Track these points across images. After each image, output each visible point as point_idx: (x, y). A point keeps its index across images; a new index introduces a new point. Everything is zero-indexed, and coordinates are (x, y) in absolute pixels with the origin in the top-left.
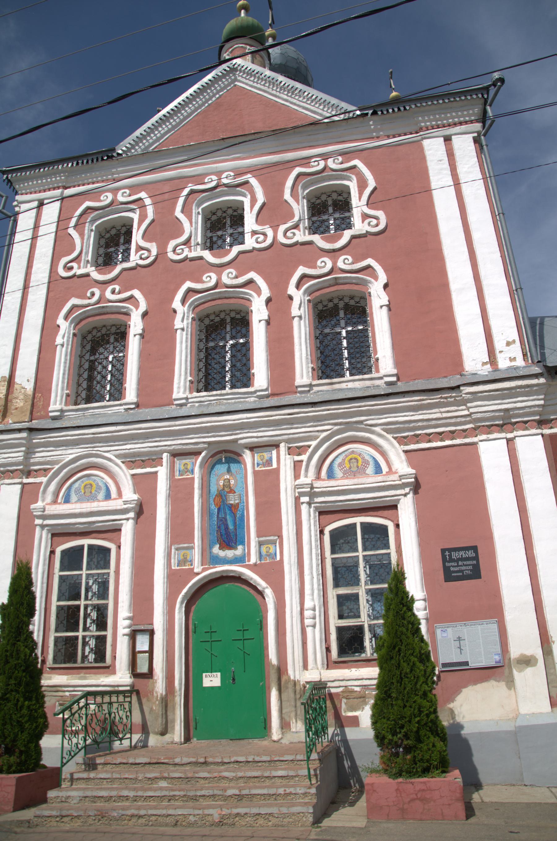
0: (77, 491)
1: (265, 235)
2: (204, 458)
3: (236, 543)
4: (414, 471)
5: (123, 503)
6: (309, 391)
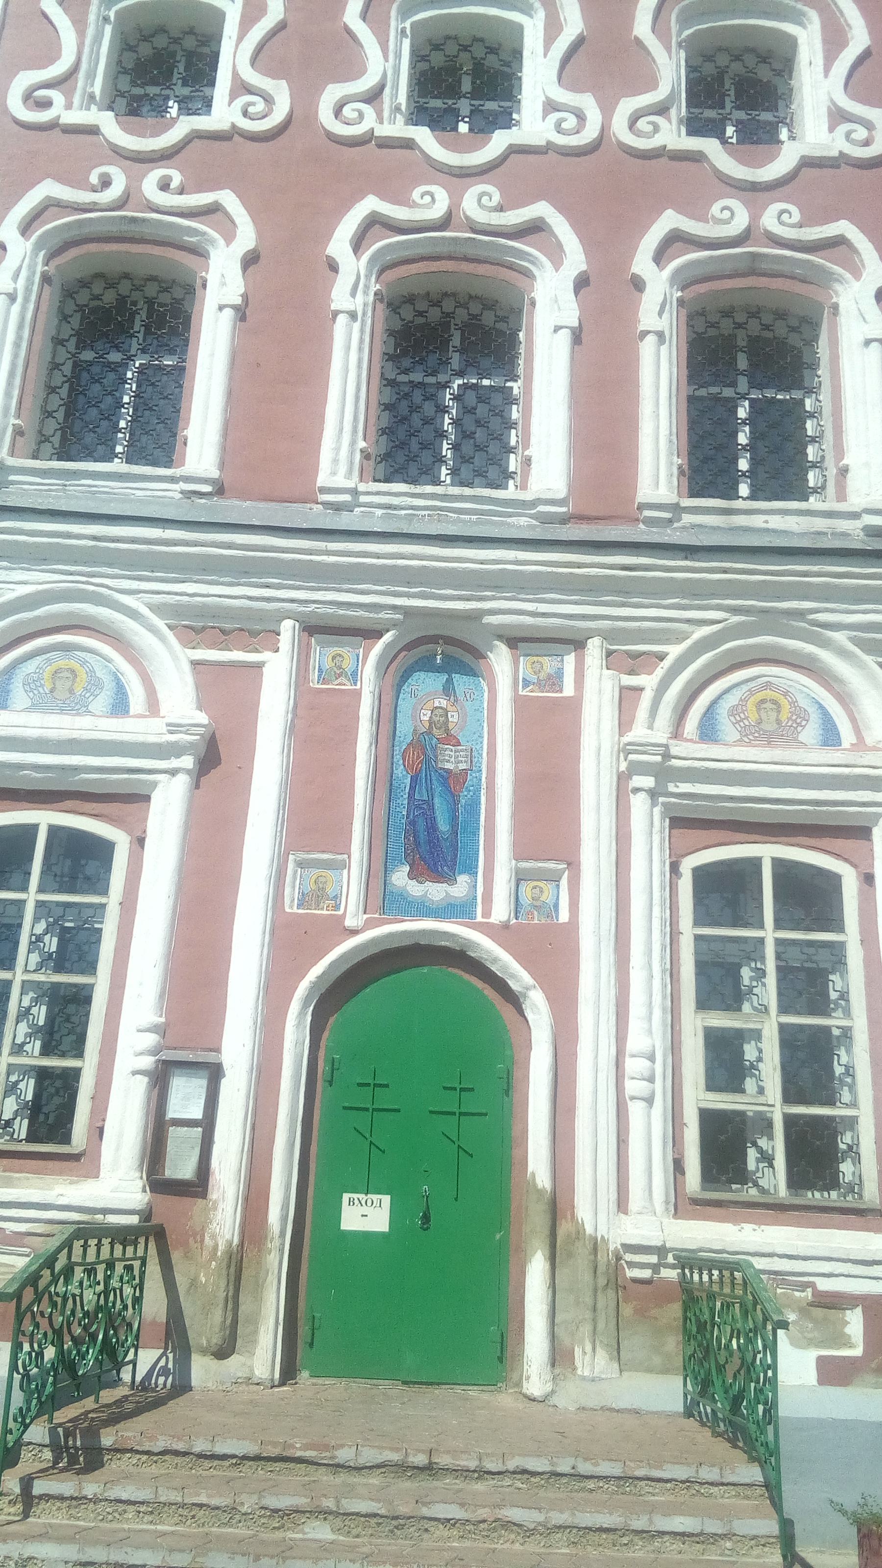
1: (581, 117)
2: (388, 646)
4: (202, 718)
5: (164, 729)
6: (670, 521)
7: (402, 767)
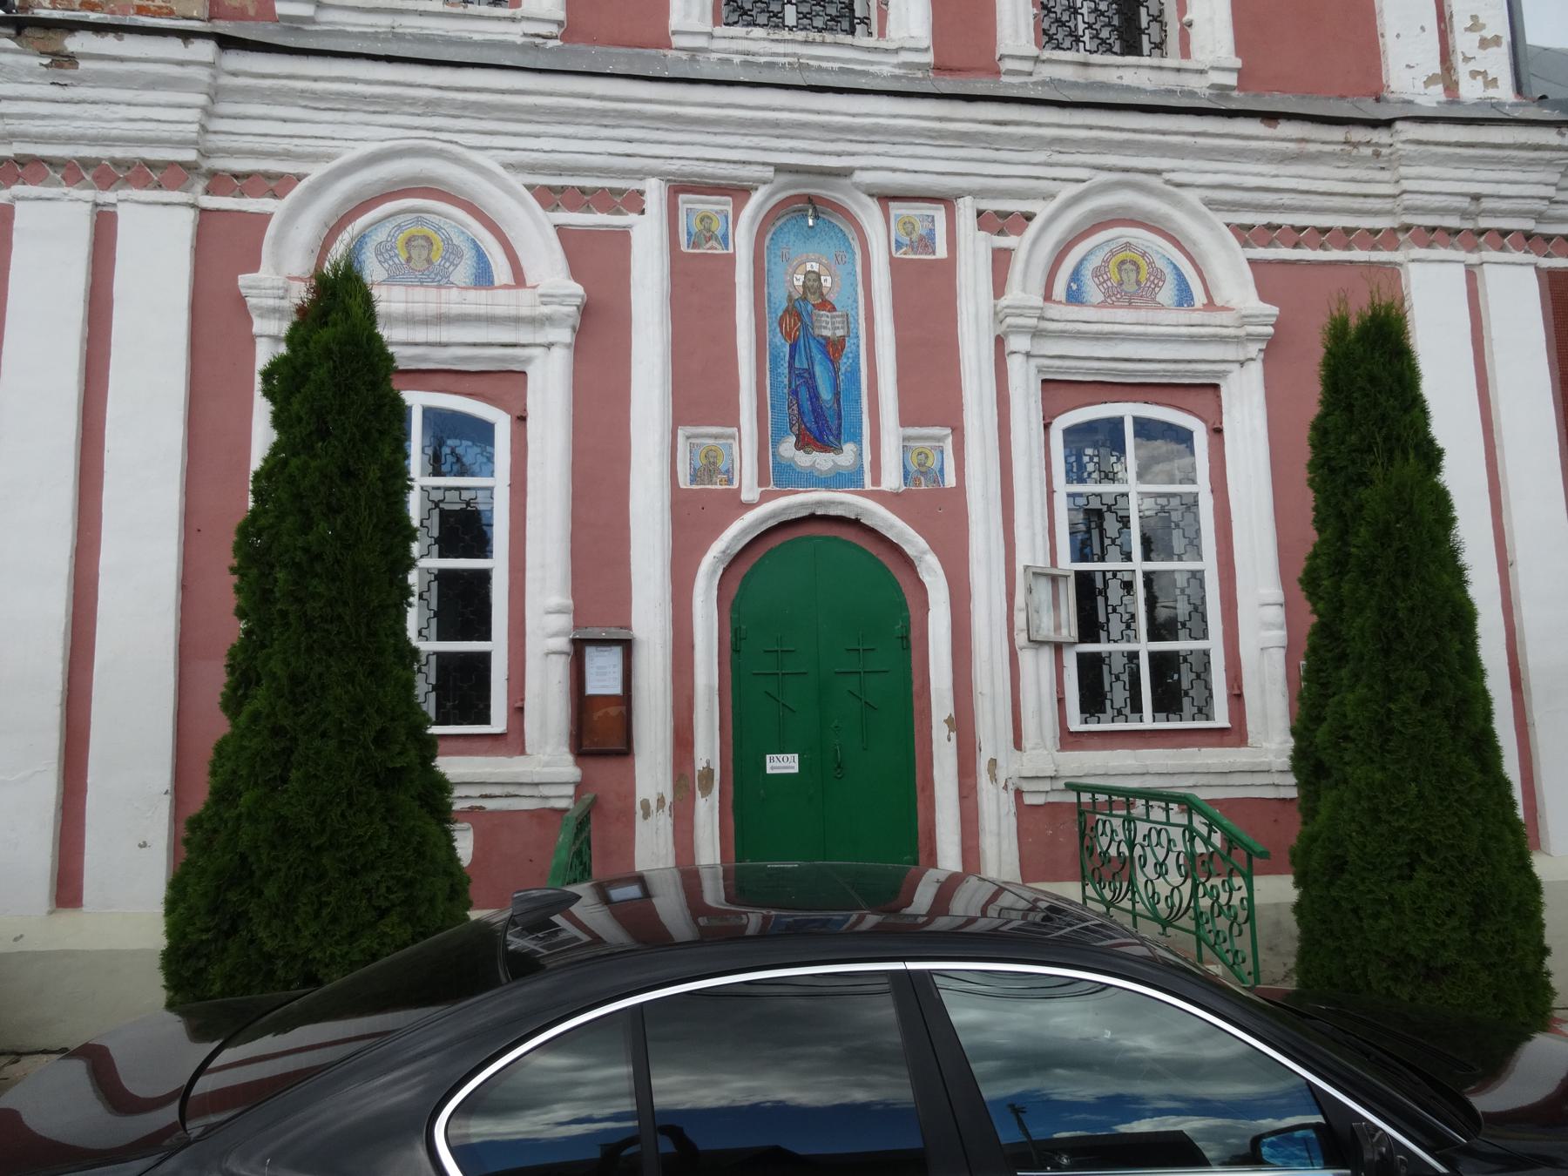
0: (383, 252)
3: (838, 437)
5: (539, 300)
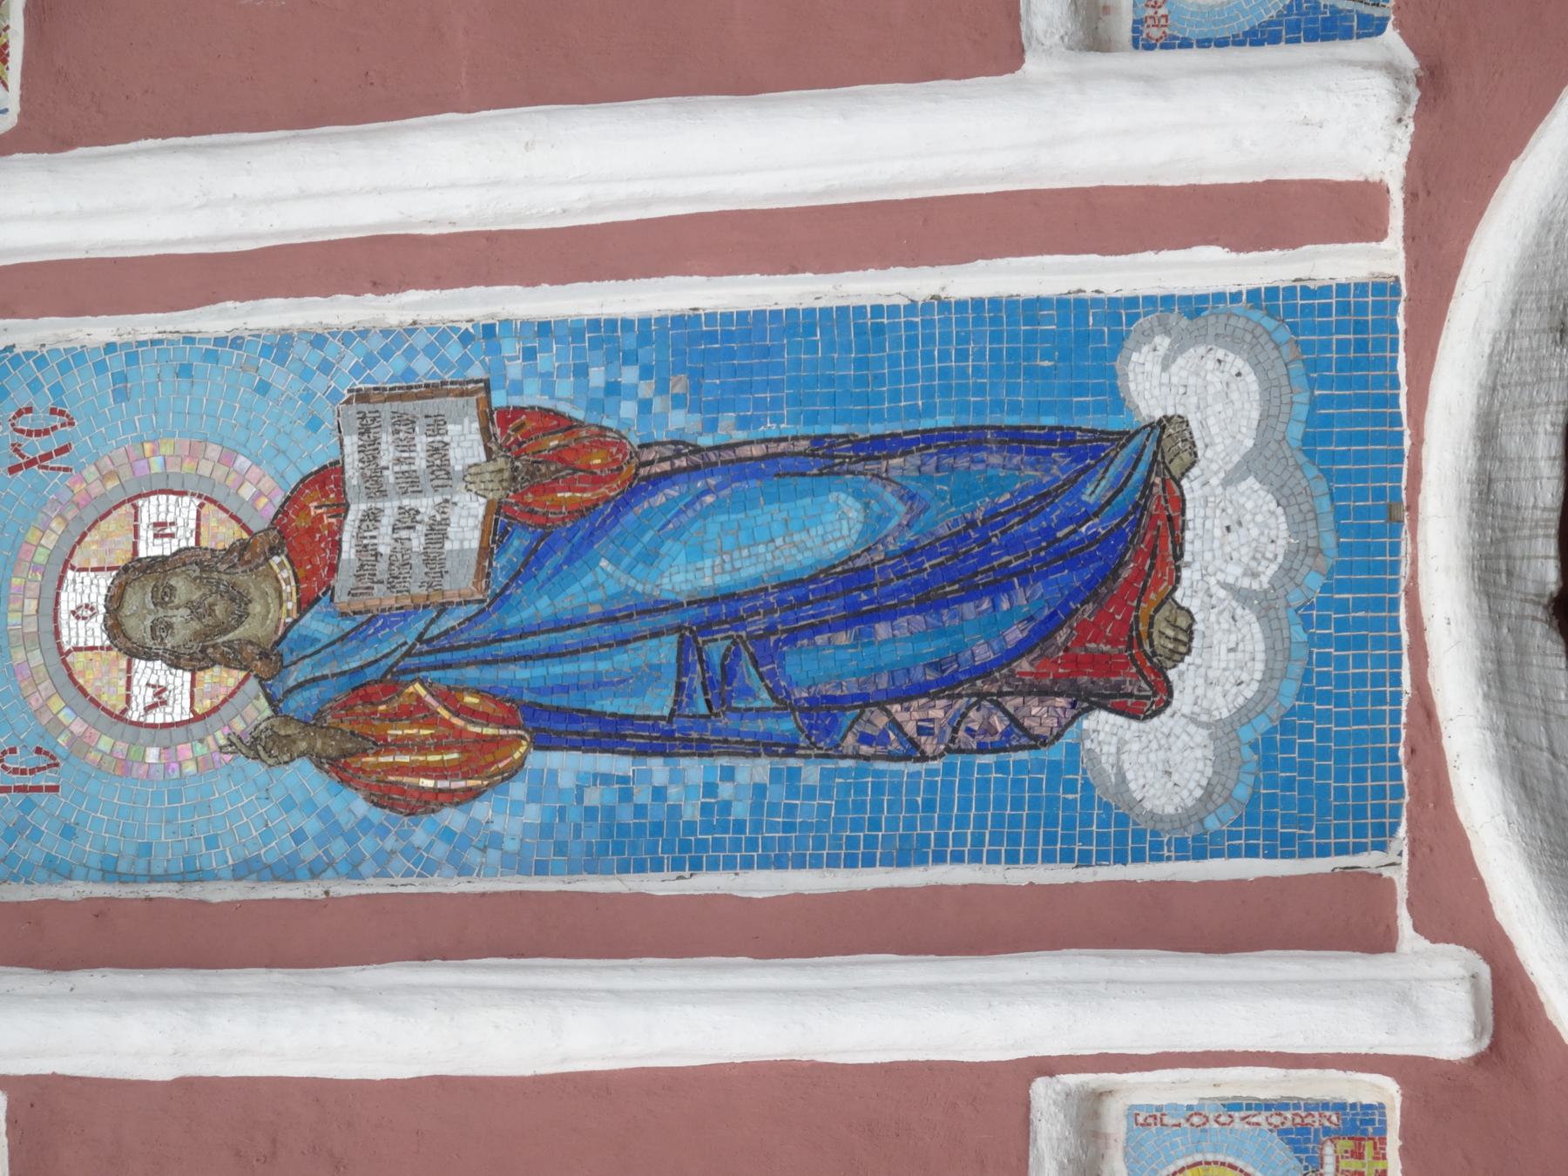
3: (1089, 449)
7: (481, 809)
